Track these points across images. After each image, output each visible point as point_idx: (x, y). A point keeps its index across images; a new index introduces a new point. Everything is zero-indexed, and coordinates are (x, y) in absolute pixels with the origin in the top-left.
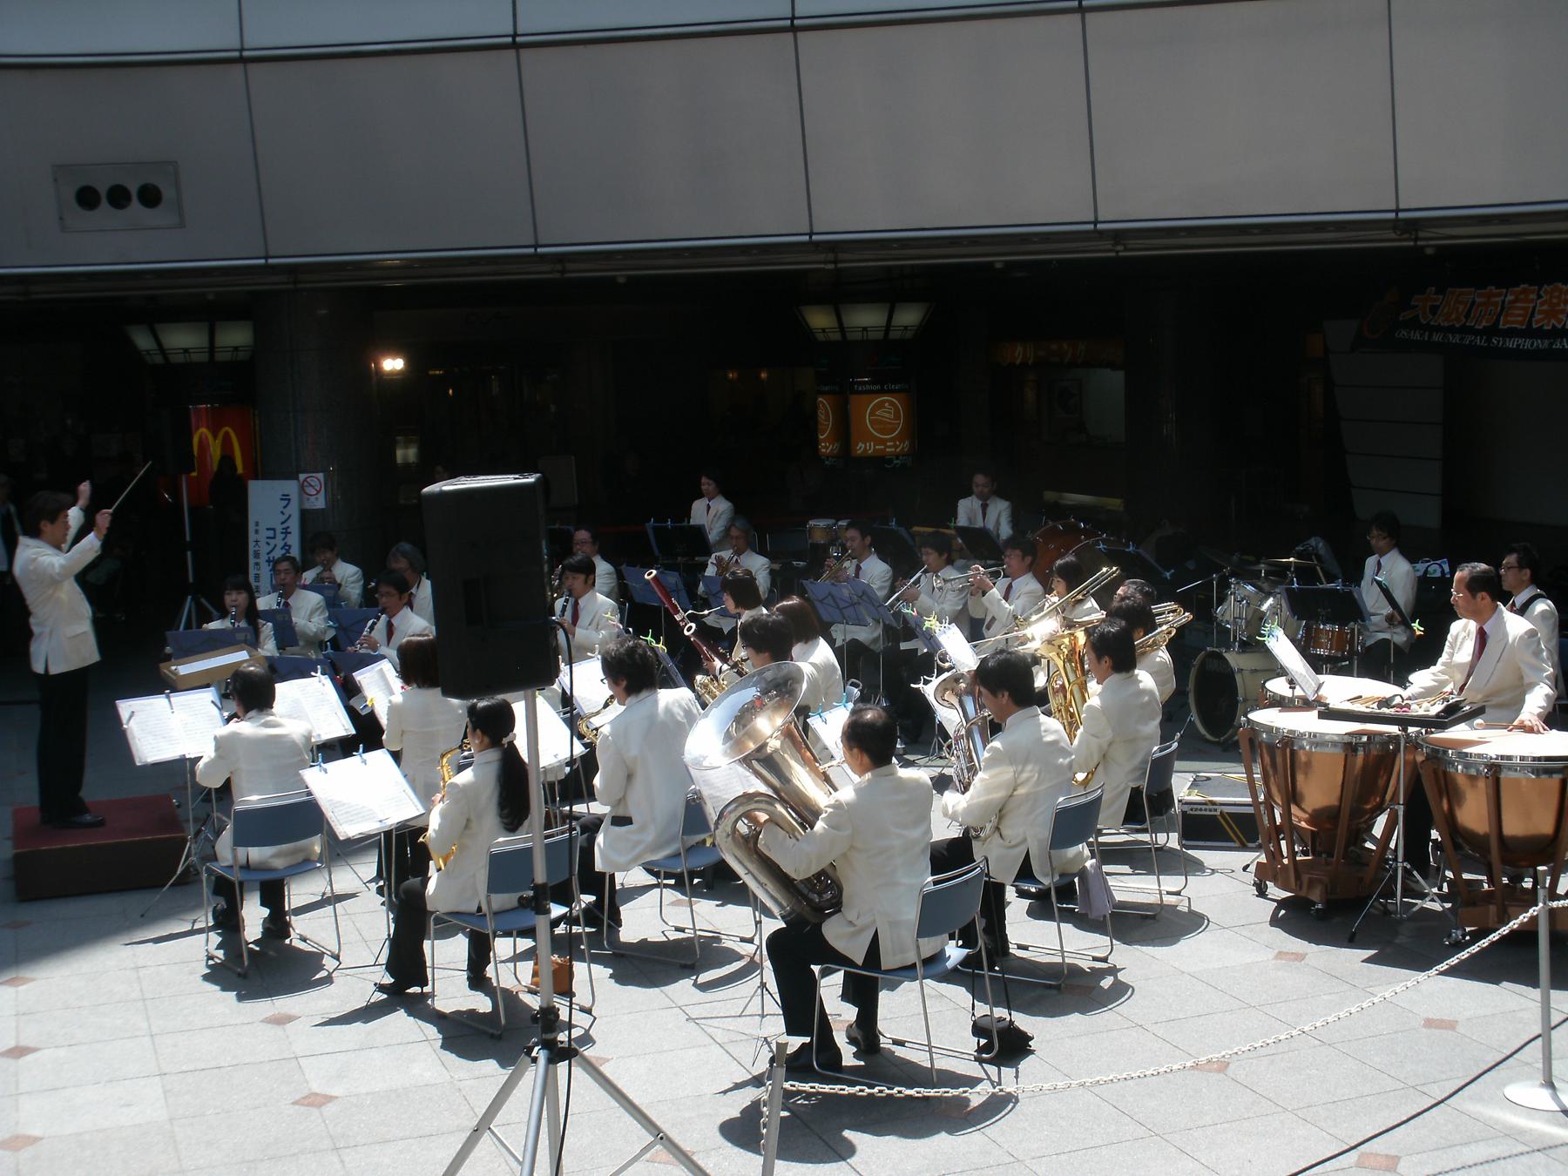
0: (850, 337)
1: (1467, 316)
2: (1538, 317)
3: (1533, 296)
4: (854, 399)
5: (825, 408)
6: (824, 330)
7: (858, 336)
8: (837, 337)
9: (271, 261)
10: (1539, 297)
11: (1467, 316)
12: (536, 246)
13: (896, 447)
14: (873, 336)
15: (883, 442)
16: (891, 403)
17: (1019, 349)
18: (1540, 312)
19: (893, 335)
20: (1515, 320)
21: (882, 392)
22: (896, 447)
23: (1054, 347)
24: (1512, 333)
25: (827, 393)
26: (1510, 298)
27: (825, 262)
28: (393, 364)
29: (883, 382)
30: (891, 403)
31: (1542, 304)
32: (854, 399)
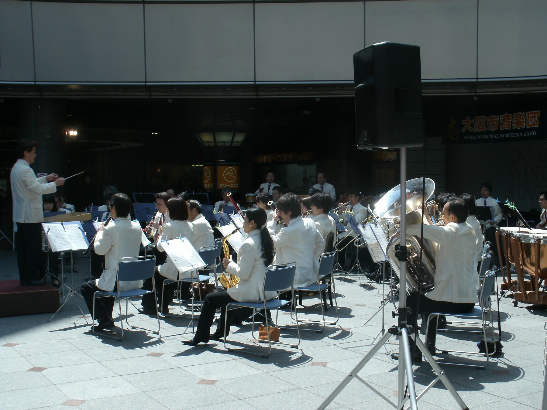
0: (218, 144)
1: (486, 126)
2: (514, 125)
3: (510, 118)
4: (219, 167)
5: (207, 172)
6: (208, 142)
7: (221, 144)
8: (213, 144)
9: (37, 83)
10: (513, 117)
11: (486, 126)
12: (146, 82)
13: (234, 185)
14: (226, 144)
15: (229, 184)
16: (233, 169)
17: (265, 157)
18: (514, 123)
19: (234, 144)
20: (506, 126)
21: (229, 165)
22: (234, 185)
23: (280, 156)
24: (506, 132)
25: (208, 165)
26: (501, 119)
27: (254, 96)
28: (73, 133)
29: (230, 161)
30: (233, 169)
31: (514, 120)
32: (219, 167)
